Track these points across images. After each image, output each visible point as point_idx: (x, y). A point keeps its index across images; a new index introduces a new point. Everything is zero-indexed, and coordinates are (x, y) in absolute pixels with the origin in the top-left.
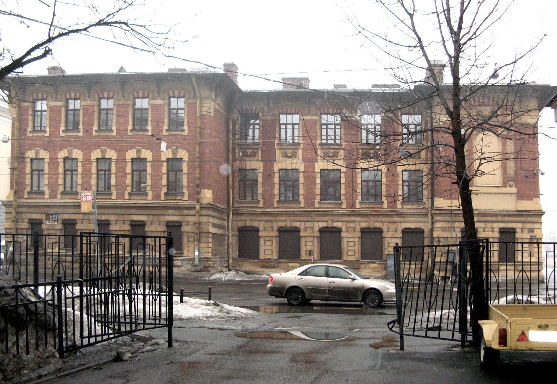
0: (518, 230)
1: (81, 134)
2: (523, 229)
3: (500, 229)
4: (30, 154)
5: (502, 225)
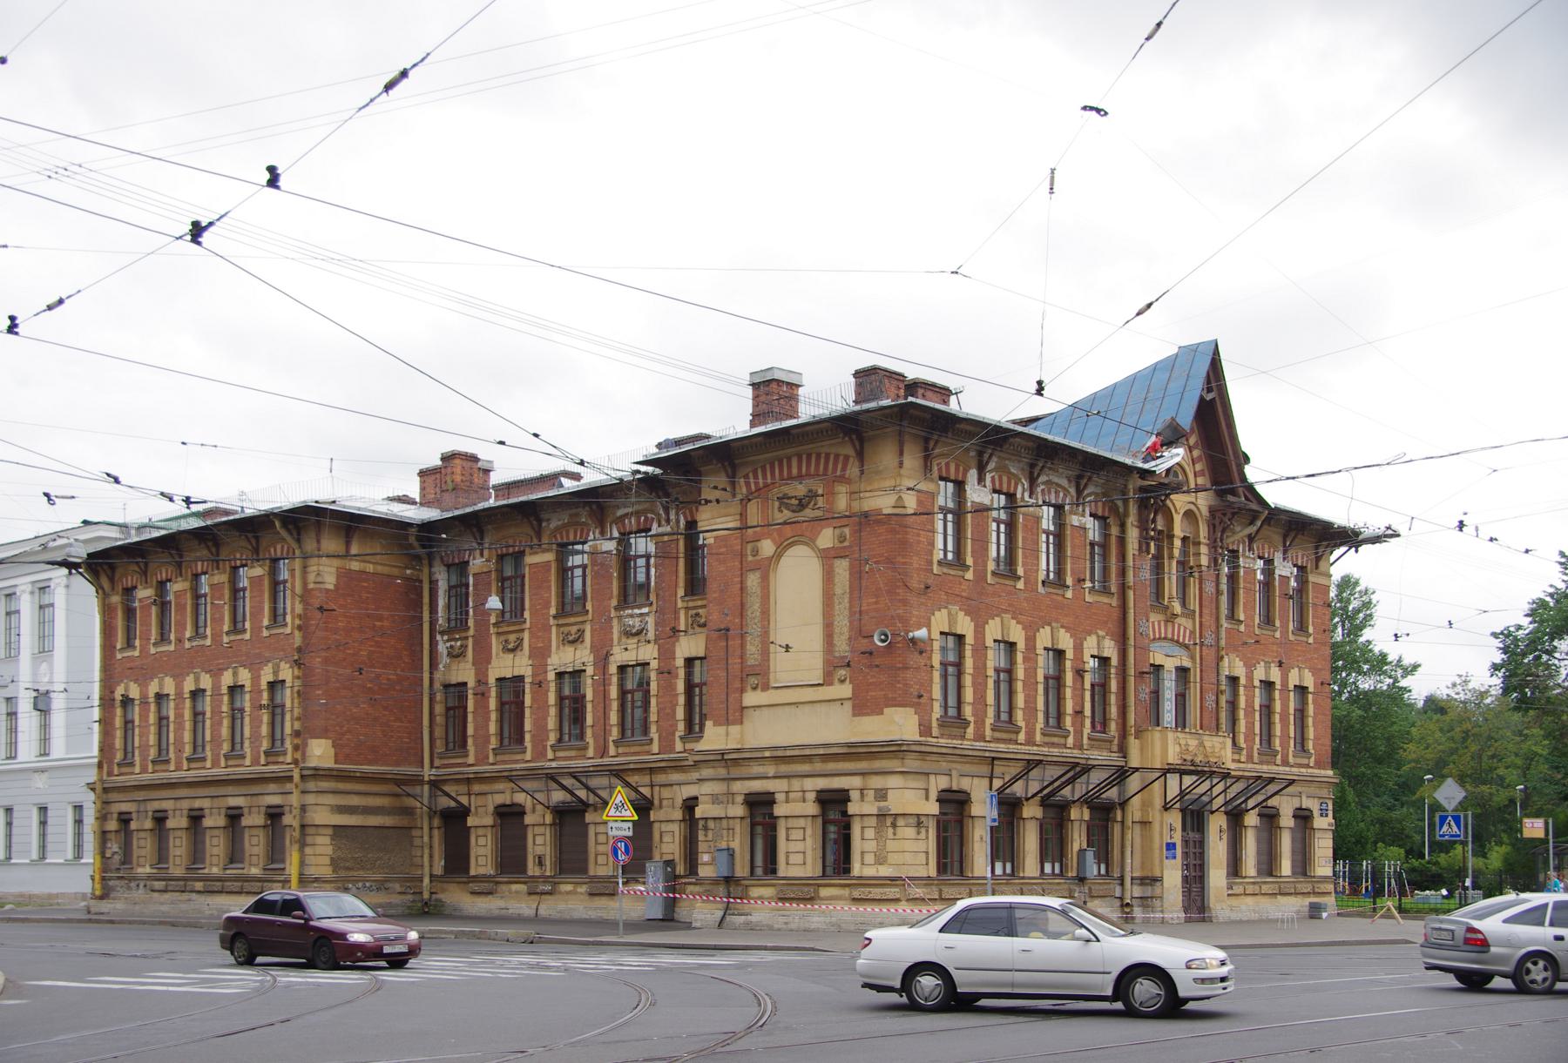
0: (854, 795)
1: (172, 648)
2: (865, 792)
3: (818, 792)
4: (119, 692)
5: (822, 783)
